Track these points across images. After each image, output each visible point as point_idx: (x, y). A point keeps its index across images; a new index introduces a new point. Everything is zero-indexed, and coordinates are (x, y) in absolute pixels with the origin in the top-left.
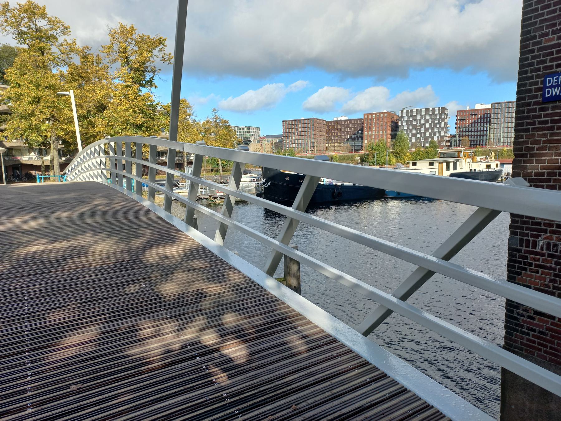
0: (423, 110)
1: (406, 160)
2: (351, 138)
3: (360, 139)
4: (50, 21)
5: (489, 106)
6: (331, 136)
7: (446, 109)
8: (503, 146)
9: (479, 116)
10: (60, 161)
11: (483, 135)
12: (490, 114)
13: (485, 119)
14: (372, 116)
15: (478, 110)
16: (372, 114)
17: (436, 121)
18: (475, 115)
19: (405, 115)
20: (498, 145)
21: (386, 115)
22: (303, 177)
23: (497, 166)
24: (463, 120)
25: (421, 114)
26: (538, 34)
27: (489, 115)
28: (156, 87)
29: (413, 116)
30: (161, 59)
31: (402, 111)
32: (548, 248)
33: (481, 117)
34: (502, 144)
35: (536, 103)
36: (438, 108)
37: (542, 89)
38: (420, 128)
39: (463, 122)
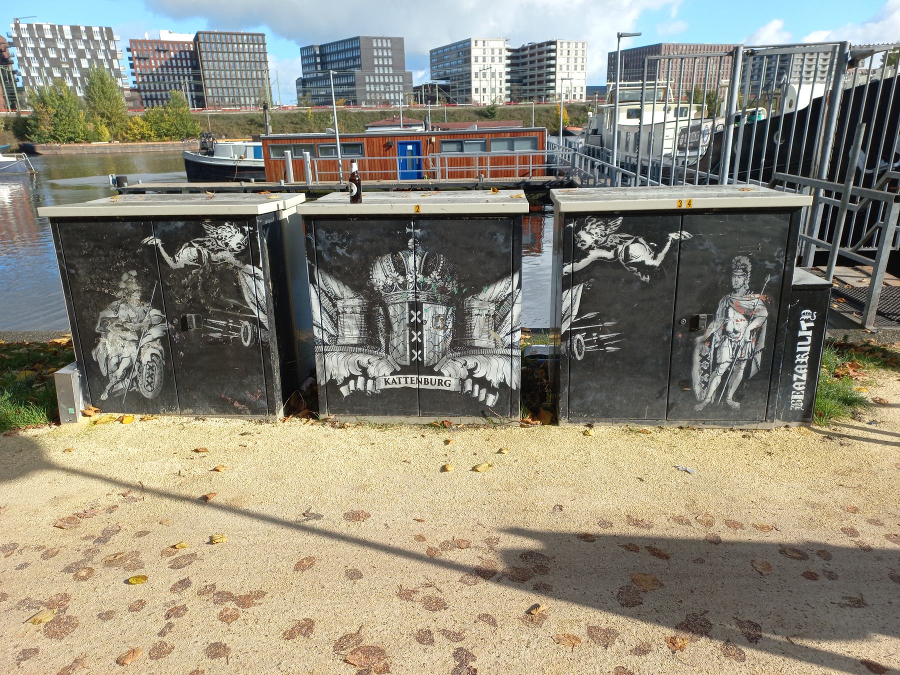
1: (136, 131)
9: (172, 54)
11: (160, 90)
15: (168, 43)
17: (101, 56)
18: (165, 51)
19: (25, 35)
22: (800, 208)
24: (145, 59)
25: (63, 38)
33: (175, 55)
38: (68, 66)
39: (145, 64)
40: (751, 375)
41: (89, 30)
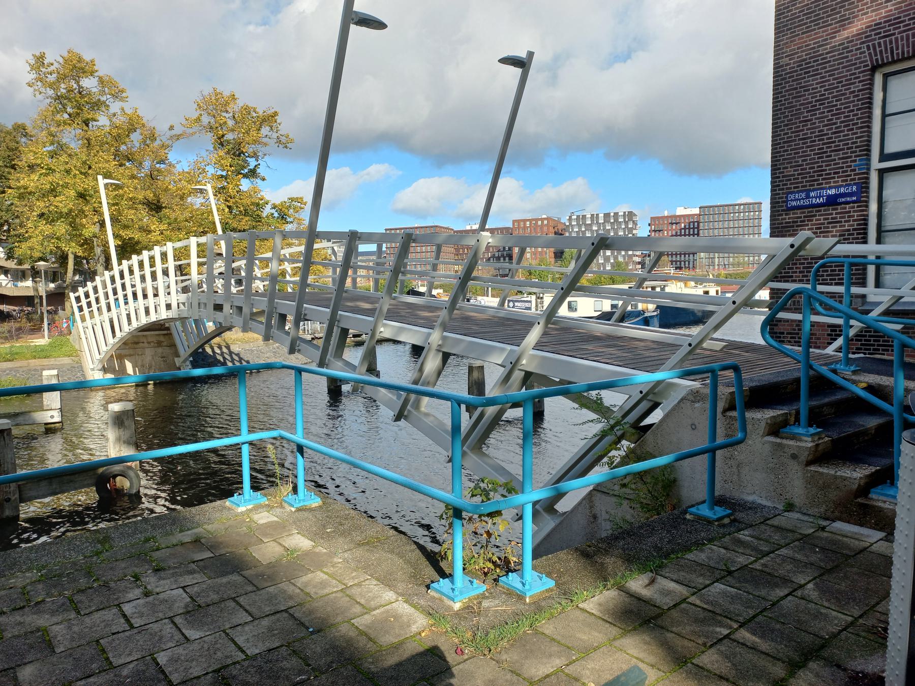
0: (601, 215)
2: (493, 256)
3: (507, 259)
4: (101, 81)
5: (696, 211)
6: (463, 254)
7: (635, 215)
8: (719, 268)
9: (683, 225)
10: (48, 289)
12: (698, 223)
13: (692, 230)
14: (525, 224)
16: (525, 221)
19: (574, 223)
20: (711, 267)
21: (546, 222)
23: (717, 292)
24: (660, 231)
25: (597, 222)
26: (782, 167)
27: (696, 224)
28: (264, 179)
29: (586, 225)
30: (275, 141)
31: (570, 217)
32: (794, 305)
33: (685, 226)
34: (716, 267)
35: (783, 211)
36: (622, 214)
37: (786, 202)
40: (642, 424)
41: (616, 214)
